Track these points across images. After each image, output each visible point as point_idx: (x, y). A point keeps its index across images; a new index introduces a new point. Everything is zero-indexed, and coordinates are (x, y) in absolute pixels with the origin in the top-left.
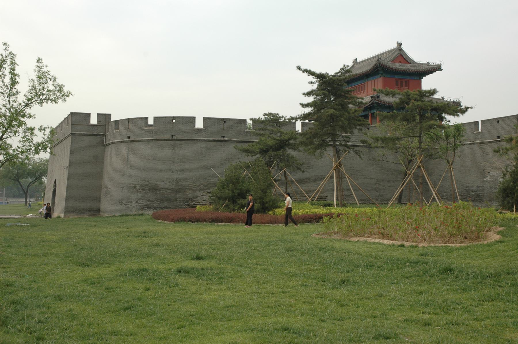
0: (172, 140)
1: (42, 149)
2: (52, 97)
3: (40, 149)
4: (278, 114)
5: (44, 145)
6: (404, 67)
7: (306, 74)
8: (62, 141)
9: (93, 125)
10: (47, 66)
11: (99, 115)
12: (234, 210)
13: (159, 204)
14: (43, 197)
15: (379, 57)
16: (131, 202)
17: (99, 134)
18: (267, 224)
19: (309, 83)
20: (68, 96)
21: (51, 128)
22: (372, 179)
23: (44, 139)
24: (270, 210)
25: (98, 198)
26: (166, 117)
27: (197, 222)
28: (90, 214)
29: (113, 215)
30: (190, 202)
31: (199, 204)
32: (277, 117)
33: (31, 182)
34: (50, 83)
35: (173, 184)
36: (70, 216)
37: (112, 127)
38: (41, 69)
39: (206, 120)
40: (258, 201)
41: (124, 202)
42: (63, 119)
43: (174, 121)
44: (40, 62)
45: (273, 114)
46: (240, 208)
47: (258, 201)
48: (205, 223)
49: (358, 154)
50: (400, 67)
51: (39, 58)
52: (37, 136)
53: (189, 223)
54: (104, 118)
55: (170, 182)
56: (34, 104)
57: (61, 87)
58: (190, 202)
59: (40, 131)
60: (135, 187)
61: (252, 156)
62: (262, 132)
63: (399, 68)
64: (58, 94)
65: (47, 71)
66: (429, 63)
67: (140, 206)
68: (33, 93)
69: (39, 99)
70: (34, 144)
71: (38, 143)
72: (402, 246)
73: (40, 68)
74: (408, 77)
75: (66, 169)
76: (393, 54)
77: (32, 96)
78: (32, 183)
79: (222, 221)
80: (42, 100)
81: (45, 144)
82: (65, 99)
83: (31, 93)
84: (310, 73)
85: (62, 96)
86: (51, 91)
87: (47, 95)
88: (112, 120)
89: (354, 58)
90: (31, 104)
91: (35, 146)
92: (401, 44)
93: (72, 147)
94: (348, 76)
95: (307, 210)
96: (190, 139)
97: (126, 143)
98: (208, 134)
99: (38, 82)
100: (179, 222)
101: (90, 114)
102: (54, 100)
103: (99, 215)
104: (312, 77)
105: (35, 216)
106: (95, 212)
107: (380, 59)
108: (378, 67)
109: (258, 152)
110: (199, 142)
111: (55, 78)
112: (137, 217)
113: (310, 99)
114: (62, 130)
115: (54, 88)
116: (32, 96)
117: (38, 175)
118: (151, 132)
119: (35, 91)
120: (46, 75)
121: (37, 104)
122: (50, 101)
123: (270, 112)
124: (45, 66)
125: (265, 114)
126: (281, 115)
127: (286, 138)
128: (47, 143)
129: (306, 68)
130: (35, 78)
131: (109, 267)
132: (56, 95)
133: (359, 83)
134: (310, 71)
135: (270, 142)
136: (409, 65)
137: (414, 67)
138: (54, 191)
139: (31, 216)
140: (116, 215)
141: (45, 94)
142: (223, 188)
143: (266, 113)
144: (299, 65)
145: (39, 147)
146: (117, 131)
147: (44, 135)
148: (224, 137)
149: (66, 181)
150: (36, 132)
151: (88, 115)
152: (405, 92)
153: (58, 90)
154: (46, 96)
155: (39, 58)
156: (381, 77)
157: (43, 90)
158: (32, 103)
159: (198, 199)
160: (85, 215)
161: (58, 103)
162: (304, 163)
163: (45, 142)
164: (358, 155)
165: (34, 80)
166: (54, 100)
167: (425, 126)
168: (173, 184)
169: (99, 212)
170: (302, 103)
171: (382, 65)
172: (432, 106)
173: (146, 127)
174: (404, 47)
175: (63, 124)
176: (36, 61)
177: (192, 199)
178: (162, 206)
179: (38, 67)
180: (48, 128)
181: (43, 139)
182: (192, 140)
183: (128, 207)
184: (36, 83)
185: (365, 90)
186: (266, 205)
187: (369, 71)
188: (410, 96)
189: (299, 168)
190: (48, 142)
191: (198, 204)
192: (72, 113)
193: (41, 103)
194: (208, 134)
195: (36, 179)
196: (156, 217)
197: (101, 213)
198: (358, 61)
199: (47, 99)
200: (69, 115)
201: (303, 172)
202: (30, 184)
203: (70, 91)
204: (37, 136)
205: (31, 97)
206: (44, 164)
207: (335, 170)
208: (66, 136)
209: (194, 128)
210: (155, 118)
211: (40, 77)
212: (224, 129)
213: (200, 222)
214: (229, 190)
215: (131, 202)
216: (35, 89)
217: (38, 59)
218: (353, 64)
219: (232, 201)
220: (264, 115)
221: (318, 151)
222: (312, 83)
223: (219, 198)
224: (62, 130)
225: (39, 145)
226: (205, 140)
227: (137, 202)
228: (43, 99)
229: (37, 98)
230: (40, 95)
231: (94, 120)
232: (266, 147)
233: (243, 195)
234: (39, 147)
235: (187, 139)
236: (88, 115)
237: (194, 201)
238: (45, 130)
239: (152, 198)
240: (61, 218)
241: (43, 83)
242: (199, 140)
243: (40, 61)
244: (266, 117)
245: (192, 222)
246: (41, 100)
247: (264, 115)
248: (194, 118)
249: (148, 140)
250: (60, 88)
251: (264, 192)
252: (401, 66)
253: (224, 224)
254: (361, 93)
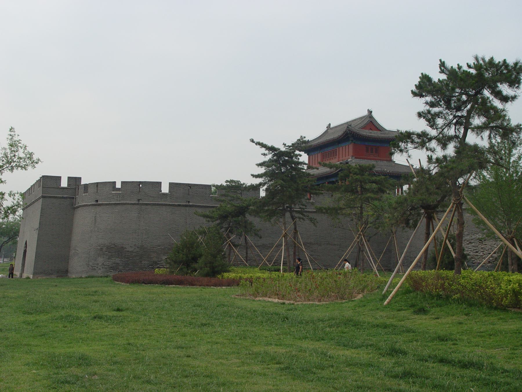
0: (138, 204)
1: (11, 213)
2: (23, 164)
3: (10, 212)
4: (239, 181)
5: (13, 209)
6: (374, 134)
7: (258, 146)
8: (34, 202)
9: (64, 188)
10: (18, 135)
11: (69, 178)
12: (187, 273)
13: (124, 266)
14: (15, 258)
15: (349, 125)
16: (98, 264)
17: (69, 197)
18: (212, 287)
19: (262, 154)
20: (37, 163)
21: (20, 193)
22: (335, 245)
23: (14, 203)
24: (220, 274)
25: (66, 259)
26: (133, 182)
27: (150, 284)
28: (58, 275)
29: (80, 276)
30: (154, 265)
31: (163, 267)
32: (239, 184)
33: (5, 242)
34: (21, 151)
35: (138, 247)
36: (39, 277)
37: (81, 190)
38: (13, 138)
39: (172, 185)
40: (208, 265)
41: (91, 264)
42: (36, 181)
43: (141, 186)
44: (13, 131)
45: (235, 181)
46: (192, 272)
47: (208, 265)
48: (157, 285)
49: (313, 221)
50: (370, 134)
51: (12, 127)
52: (7, 200)
53: (143, 284)
54: (74, 181)
55: (135, 245)
56: (5, 171)
57: (31, 154)
58: (154, 265)
59: (10, 196)
60: (101, 249)
61: (213, 221)
62: (223, 198)
63: (369, 135)
64: (28, 161)
65: (18, 140)
66: (398, 131)
67: (106, 268)
68: (5, 160)
69: (10, 166)
70: (4, 208)
71: (8, 207)
72: (284, 303)
73: (13, 137)
74: (378, 144)
75: (36, 231)
76: (363, 121)
77: (3, 164)
78: (5, 243)
79: (172, 284)
80: (13, 167)
81: (14, 208)
82: (34, 166)
83: (3, 161)
84: (262, 145)
85: (32, 163)
86: (22, 158)
87: (18, 162)
88: (82, 184)
89: (328, 124)
90: (2, 171)
91: (5, 210)
92: (371, 112)
93: (42, 209)
94: (304, 147)
95: (251, 275)
96: (155, 204)
97: (94, 207)
98: (174, 199)
99: (10, 149)
100: (134, 283)
101: (60, 177)
102: (23, 167)
103: (67, 276)
104: (264, 149)
105: (6, 276)
106: (63, 273)
107: (350, 126)
108: (348, 134)
109: (217, 218)
110: (164, 207)
111: (26, 146)
112: (100, 279)
113: (262, 170)
114: (34, 192)
115: (25, 156)
116: (3, 164)
117: (12, 235)
118: (119, 196)
119: (7, 159)
120: (18, 143)
121: (8, 171)
122: (20, 168)
123: (231, 179)
124: (17, 135)
125: (227, 181)
126: (242, 183)
127: (245, 205)
128: (16, 207)
129: (259, 141)
130: (7, 147)
131: (47, 315)
132: (26, 162)
133: (330, 149)
134: (262, 143)
135: (229, 208)
136: (379, 132)
137: (384, 134)
138: (25, 252)
139: (2, 276)
140: (83, 277)
141: (15, 161)
142: (179, 253)
143: (228, 180)
144: (252, 138)
145: (9, 211)
146: (86, 194)
147: (14, 199)
148: (189, 202)
149: (36, 242)
150: (6, 196)
151: (59, 178)
152: (347, 166)
153: (28, 157)
154: (16, 163)
155: (12, 127)
156: (351, 143)
157: (14, 158)
158: (3, 170)
159: (162, 262)
160: (53, 276)
161: (27, 170)
162: (260, 230)
163: (14, 206)
164: (313, 223)
165: (6, 148)
166: (23, 167)
167: (363, 198)
168: (138, 247)
169: (67, 274)
170: (252, 174)
171: (352, 132)
172: (370, 180)
173: (113, 191)
174: (374, 115)
175: (35, 186)
176: (9, 130)
177: (156, 262)
178: (127, 269)
179: (10, 135)
180: (18, 193)
181: (13, 204)
182: (158, 205)
183: (95, 269)
184: (8, 151)
185: (336, 155)
186: (216, 269)
187: (340, 137)
188: (351, 170)
189: (257, 234)
190: (17, 206)
191: (162, 267)
192: (43, 176)
193: (12, 169)
194: (174, 199)
195: (10, 239)
196: (116, 279)
197: (69, 275)
198: (331, 126)
199: (17, 166)
200: (41, 178)
201: (261, 238)
202: (3, 243)
203: (39, 158)
204: (7, 200)
205: (2, 164)
206: (18, 223)
207: (284, 237)
208: (38, 198)
209: (160, 193)
210: (123, 183)
211: (11, 145)
212: (189, 194)
213: (152, 284)
214: (183, 254)
215: (98, 264)
216: (7, 157)
217: (10, 128)
218: (326, 129)
219: (186, 265)
220: (226, 182)
221: (275, 218)
222: (264, 155)
223: (175, 262)
224: (34, 192)
225: (9, 208)
226: (170, 205)
227: (103, 264)
228: (13, 166)
229: (8, 165)
230: (11, 162)
231: (64, 183)
232: (226, 214)
233: (195, 259)
234: (9, 211)
235: (153, 204)
236: (59, 178)
237: (158, 264)
238: (14, 195)
239: (118, 260)
240: (30, 278)
241: (14, 151)
242: (164, 204)
243: (13, 130)
244: (228, 183)
245: (146, 284)
246: (12, 166)
247: (226, 182)
248: (160, 183)
249: (115, 203)
250: (30, 156)
251: (215, 257)
252: (371, 133)
253: (174, 286)
254: (330, 159)
